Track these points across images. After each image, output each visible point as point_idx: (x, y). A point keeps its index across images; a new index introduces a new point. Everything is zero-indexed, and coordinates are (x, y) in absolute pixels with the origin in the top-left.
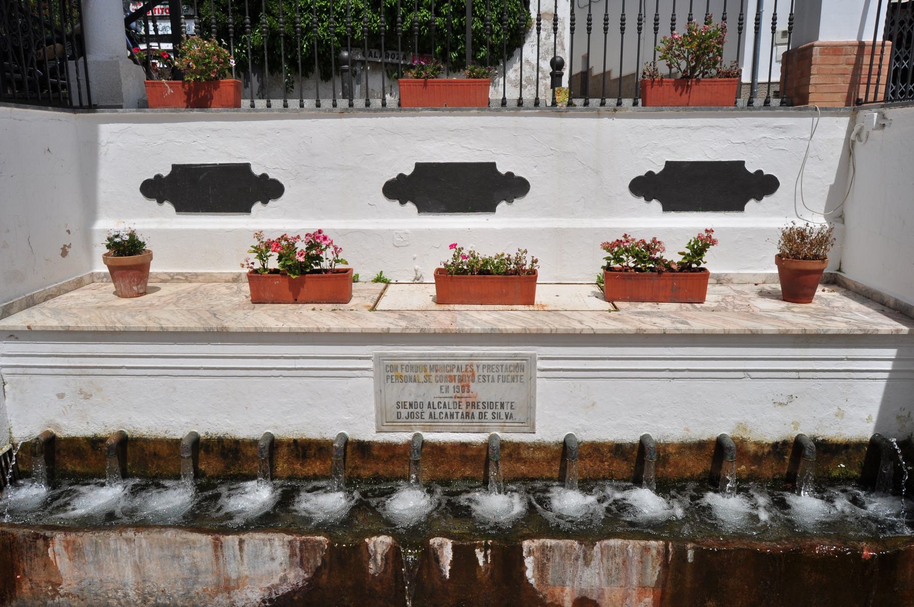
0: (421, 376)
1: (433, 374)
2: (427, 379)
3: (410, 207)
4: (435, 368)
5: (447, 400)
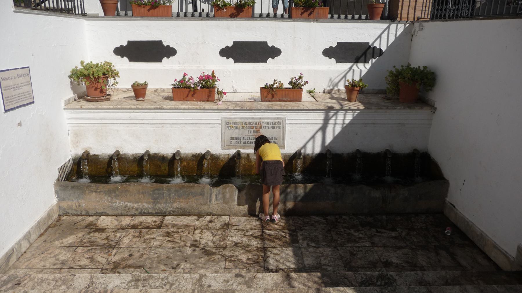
0: (241, 127)
1: (245, 126)
2: (243, 128)
3: (231, 60)
4: (245, 123)
5: (250, 136)
